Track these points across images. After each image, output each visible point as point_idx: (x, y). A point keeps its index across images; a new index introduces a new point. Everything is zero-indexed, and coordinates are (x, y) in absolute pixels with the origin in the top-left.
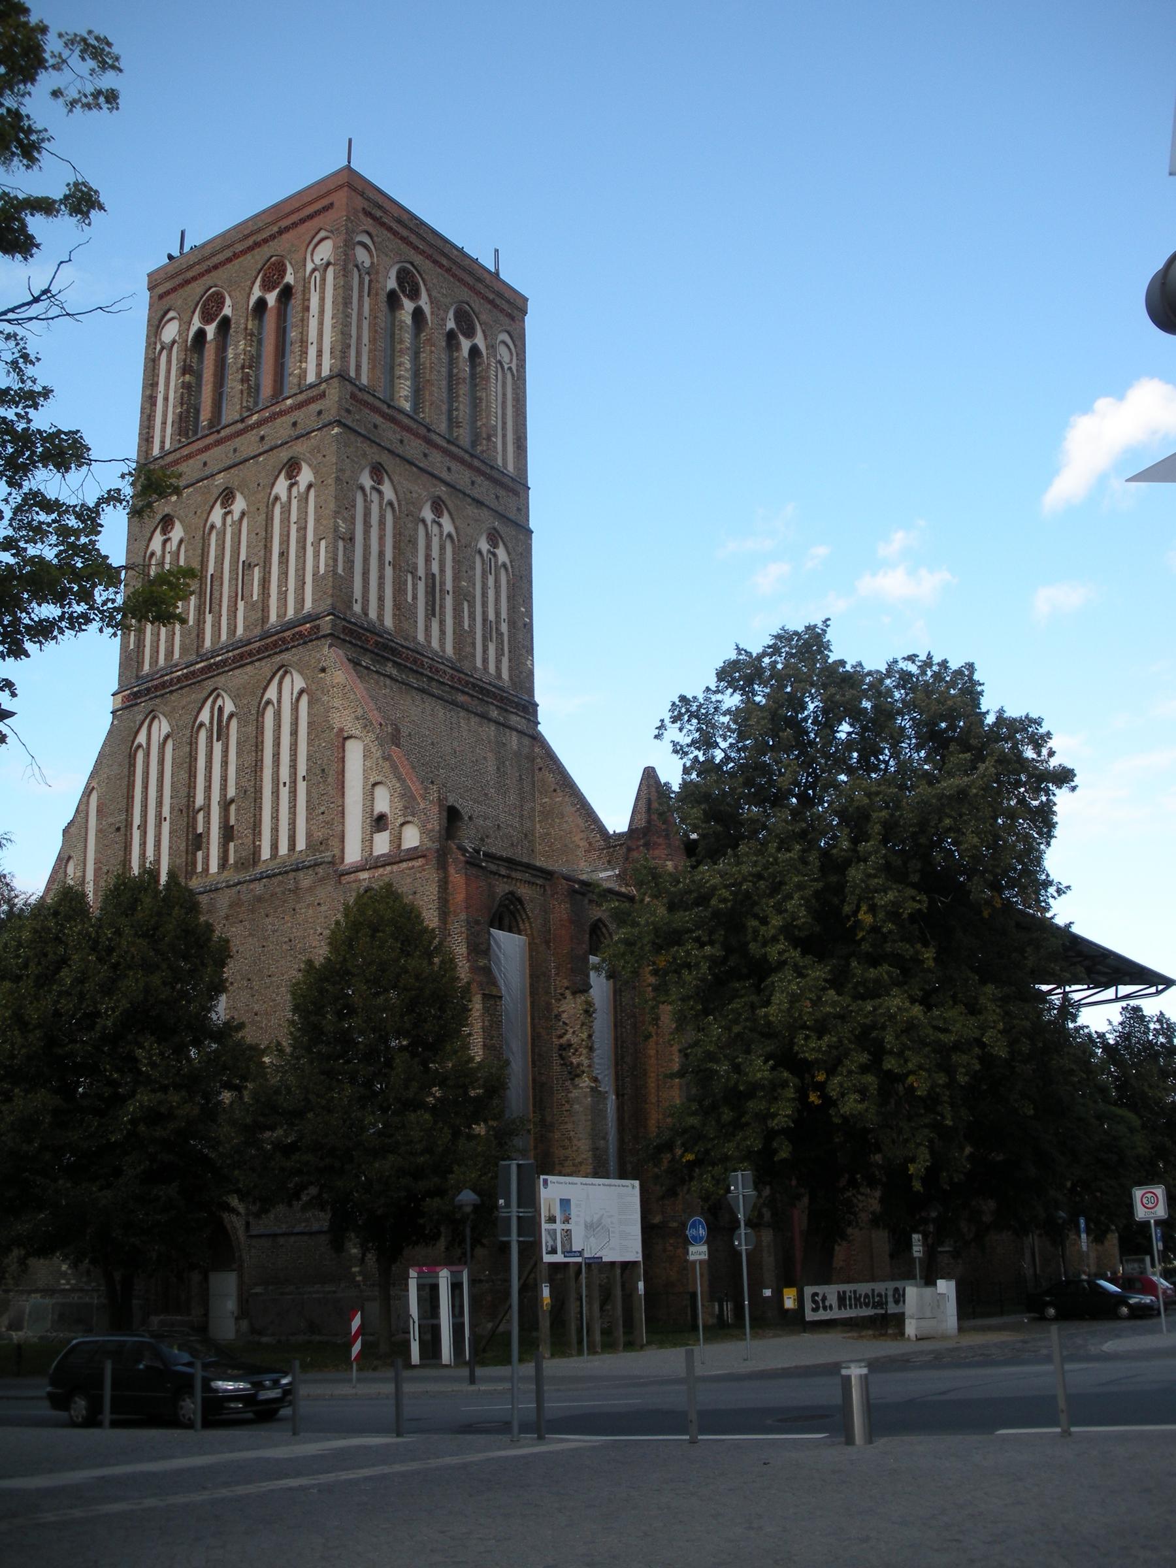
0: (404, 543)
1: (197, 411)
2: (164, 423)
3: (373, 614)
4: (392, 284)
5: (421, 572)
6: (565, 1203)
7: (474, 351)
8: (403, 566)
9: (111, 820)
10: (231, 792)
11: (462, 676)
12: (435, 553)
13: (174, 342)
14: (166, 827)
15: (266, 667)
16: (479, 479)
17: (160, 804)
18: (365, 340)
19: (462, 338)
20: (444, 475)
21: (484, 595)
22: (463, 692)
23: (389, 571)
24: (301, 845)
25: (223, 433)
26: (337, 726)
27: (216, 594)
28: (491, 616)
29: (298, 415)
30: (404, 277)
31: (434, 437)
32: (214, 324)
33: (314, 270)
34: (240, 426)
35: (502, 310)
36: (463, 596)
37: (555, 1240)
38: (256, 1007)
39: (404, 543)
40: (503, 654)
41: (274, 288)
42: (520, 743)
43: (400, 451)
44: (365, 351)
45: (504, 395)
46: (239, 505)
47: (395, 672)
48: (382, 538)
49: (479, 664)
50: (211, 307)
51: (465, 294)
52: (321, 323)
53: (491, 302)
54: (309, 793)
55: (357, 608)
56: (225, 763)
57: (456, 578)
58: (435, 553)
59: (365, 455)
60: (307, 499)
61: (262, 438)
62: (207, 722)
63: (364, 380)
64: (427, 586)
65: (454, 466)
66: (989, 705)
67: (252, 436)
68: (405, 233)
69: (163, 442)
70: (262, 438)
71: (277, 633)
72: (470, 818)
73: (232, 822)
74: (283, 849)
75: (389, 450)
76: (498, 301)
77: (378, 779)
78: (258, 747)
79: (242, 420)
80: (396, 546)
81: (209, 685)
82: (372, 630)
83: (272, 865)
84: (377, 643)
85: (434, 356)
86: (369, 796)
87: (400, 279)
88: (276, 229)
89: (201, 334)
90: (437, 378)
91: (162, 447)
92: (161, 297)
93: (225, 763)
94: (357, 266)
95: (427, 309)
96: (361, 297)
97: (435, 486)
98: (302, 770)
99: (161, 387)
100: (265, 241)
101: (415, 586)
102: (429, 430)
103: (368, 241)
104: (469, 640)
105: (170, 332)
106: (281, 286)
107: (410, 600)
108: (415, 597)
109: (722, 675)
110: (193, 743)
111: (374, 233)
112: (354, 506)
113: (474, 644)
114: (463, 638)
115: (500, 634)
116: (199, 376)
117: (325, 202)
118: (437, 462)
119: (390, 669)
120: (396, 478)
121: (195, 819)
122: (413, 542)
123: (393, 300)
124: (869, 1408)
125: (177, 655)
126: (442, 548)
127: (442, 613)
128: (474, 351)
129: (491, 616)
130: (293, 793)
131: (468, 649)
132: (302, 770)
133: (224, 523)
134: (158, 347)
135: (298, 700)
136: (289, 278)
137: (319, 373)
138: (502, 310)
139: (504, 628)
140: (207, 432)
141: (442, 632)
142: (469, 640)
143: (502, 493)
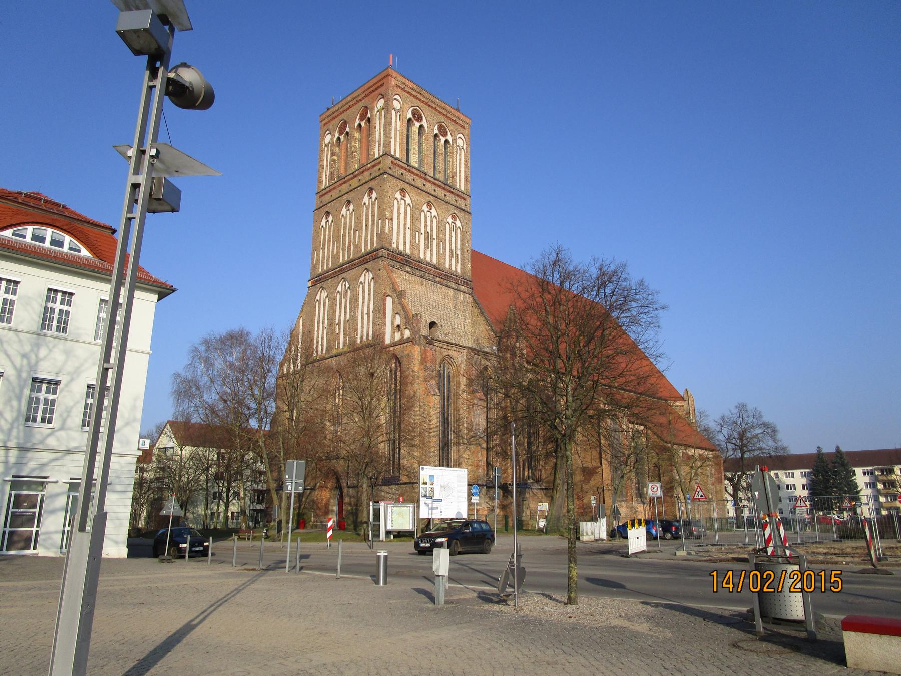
0: (415, 220)
5: (423, 231)
7: (447, 142)
8: (415, 229)
10: (348, 318)
16: (448, 194)
18: (398, 139)
20: (433, 193)
23: (408, 231)
28: (453, 248)
29: (372, 170)
35: (459, 125)
36: (440, 240)
39: (415, 220)
51: (442, 119)
55: (395, 246)
57: (438, 233)
63: (398, 156)
74: (365, 339)
78: (357, 300)
80: (412, 222)
82: (400, 254)
85: (428, 145)
86: (393, 318)
96: (396, 121)
101: (419, 237)
108: (419, 241)
110: (335, 299)
117: (381, 83)
119: (408, 269)
122: (419, 220)
126: (432, 222)
127: (432, 248)
128: (447, 142)
129: (453, 248)
130: (369, 317)
131: (442, 261)
132: (372, 310)
136: (369, 115)
138: (459, 125)
139: (459, 252)
141: (432, 255)
143: (458, 199)
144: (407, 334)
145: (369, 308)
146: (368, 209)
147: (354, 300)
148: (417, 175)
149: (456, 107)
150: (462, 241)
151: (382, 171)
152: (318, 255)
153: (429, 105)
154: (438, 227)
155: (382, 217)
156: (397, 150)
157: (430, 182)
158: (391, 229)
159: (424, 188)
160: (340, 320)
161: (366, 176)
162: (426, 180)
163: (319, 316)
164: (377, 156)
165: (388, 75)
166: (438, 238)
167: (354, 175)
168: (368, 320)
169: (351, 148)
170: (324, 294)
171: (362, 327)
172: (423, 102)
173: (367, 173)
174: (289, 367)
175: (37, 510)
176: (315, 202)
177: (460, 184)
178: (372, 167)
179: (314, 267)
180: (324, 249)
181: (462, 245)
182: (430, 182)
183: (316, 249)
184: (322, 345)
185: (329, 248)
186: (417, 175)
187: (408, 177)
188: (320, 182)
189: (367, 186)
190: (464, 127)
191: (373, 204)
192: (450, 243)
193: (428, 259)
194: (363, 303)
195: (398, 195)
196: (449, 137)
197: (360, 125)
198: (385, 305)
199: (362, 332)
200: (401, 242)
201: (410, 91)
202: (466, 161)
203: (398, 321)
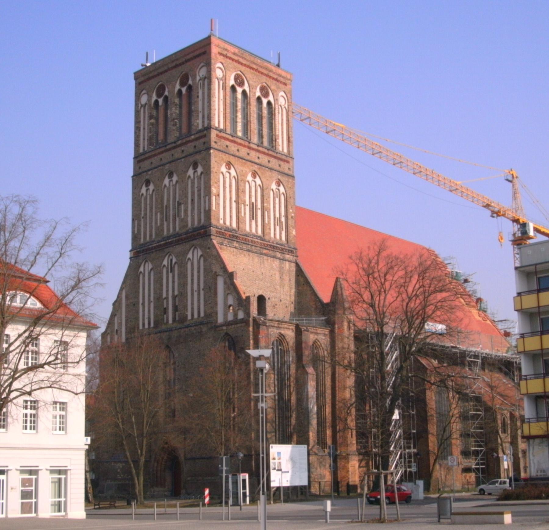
1: (157, 134)
2: (144, 139)
4: (232, 82)
5: (247, 202)
6: (279, 453)
7: (269, 103)
9: (131, 301)
10: (176, 293)
11: (265, 242)
13: (146, 104)
14: (152, 305)
15: (187, 246)
16: (272, 159)
17: (149, 296)
20: (257, 161)
21: (274, 207)
22: (265, 249)
24: (202, 315)
25: (168, 147)
26: (214, 271)
27: (168, 214)
29: (196, 143)
30: (237, 78)
33: (200, 80)
34: (174, 145)
35: (281, 82)
37: (275, 465)
38: (187, 375)
40: (283, 230)
42: (290, 266)
45: (282, 120)
46: (175, 178)
47: (237, 245)
50: (160, 92)
51: (264, 79)
52: (203, 104)
53: (276, 80)
54: (205, 295)
55: (221, 222)
56: (173, 282)
57: (263, 202)
59: (223, 159)
60: (201, 178)
61: (183, 151)
62: (166, 265)
63: (222, 127)
64: (250, 208)
65: (261, 156)
66: (449, 269)
67: (179, 150)
69: (144, 147)
70: (183, 151)
71: (191, 232)
72: (269, 299)
73: (177, 304)
74: (196, 316)
75: (233, 155)
76: (279, 78)
77: (229, 292)
78: (185, 276)
79: (175, 142)
81: (167, 250)
82: (227, 229)
83: (192, 322)
84: (230, 235)
87: (236, 79)
88: (184, 60)
89: (157, 102)
91: (144, 149)
93: (173, 282)
97: (252, 166)
98: (202, 286)
99: (142, 123)
101: (245, 209)
103: (221, 66)
104: (268, 227)
105: (144, 99)
106: (187, 85)
108: (245, 214)
110: (161, 273)
111: (224, 62)
112: (219, 182)
113: (270, 229)
115: (281, 222)
116: (157, 119)
119: (235, 244)
120: (236, 166)
121: (163, 302)
122: (244, 191)
124: (330, 516)
125: (154, 237)
128: (269, 103)
132: (202, 286)
133: (170, 185)
134: (140, 105)
135: (200, 259)
136: (190, 82)
137: (203, 126)
138: (281, 82)
139: (283, 219)
140: (161, 145)
141: (257, 225)
142: (268, 227)
143: (281, 163)
146: (193, 182)
147: (183, 275)
149: (276, 63)
153: (251, 68)
158: (218, 204)
159: (248, 158)
160: (167, 294)
161: (189, 148)
162: (250, 148)
163: (144, 289)
164: (200, 127)
166: (263, 207)
170: (149, 266)
171: (192, 304)
172: (245, 65)
174: (112, 339)
175: (33, 488)
178: (197, 139)
180: (145, 217)
184: (149, 319)
185: (151, 218)
187: (233, 148)
189: (192, 159)
191: (200, 178)
193: (252, 184)
194: (192, 280)
195: (224, 169)
196: (271, 98)
197: (180, 91)
198: (216, 284)
199: (192, 309)
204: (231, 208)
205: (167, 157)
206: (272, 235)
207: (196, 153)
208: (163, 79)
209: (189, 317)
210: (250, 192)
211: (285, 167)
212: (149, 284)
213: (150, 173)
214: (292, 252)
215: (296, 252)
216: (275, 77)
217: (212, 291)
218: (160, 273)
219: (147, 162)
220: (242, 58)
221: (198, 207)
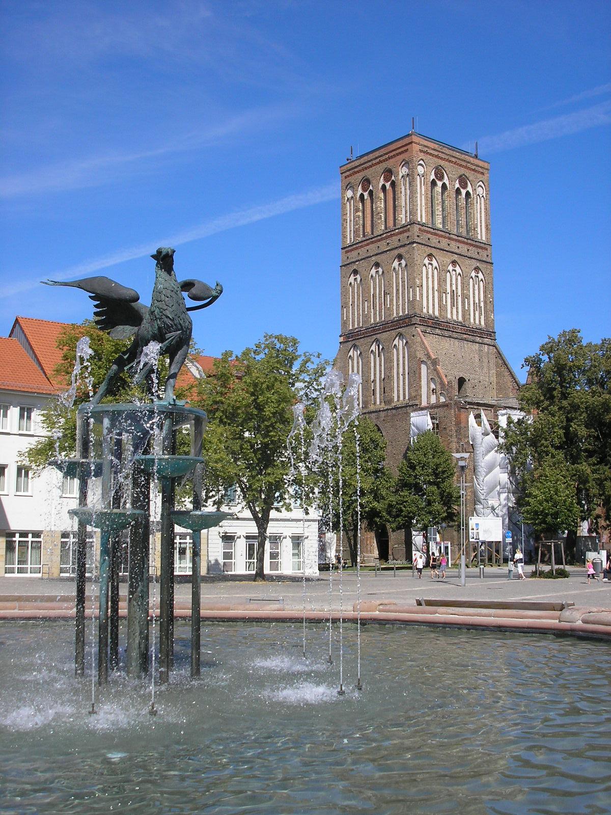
0: (442, 281)
3: (431, 312)
5: (449, 290)
6: (477, 525)
7: (468, 194)
8: (442, 291)
12: (454, 282)
18: (423, 204)
19: (462, 190)
21: (474, 294)
22: (465, 334)
23: (436, 293)
28: (477, 301)
31: (452, 236)
32: (367, 192)
36: (465, 297)
39: (442, 281)
41: (389, 181)
43: (438, 246)
44: (424, 208)
48: (433, 282)
49: (472, 320)
50: (366, 182)
51: (462, 171)
53: (474, 170)
55: (425, 311)
57: (463, 289)
58: (454, 282)
63: (424, 221)
65: (460, 245)
68: (436, 153)
74: (401, 398)
78: (392, 361)
80: (439, 284)
82: (431, 318)
85: (450, 202)
90: (452, 210)
92: (346, 177)
94: (418, 175)
95: (447, 183)
96: (421, 187)
97: (453, 256)
100: (384, 161)
101: (446, 297)
102: (450, 234)
107: (444, 303)
108: (446, 302)
109: (542, 348)
113: (470, 314)
114: (465, 313)
115: (480, 307)
117: (405, 148)
118: (454, 246)
122: (445, 281)
123: (434, 183)
126: (457, 279)
127: (457, 305)
128: (468, 194)
129: (477, 301)
131: (468, 317)
139: (482, 304)
141: (457, 312)
143: (480, 250)
144: (442, 399)
145: (404, 369)
147: (389, 361)
148: (442, 236)
150: (485, 292)
151: (410, 240)
152: (348, 312)
153: (450, 161)
154: (462, 283)
155: (412, 286)
156: (422, 216)
157: (453, 240)
158: (421, 295)
161: (394, 241)
165: (411, 143)
166: (463, 294)
167: (380, 238)
168: (404, 381)
169: (376, 208)
173: (395, 238)
176: (338, 258)
177: (481, 235)
178: (401, 233)
179: (345, 324)
181: (485, 296)
182: (453, 240)
183: (344, 306)
186: (442, 236)
187: (434, 240)
188: (345, 237)
189: (396, 252)
190: (483, 174)
192: (474, 297)
193: (455, 317)
196: (469, 188)
200: (429, 306)
201: (432, 152)
202: (486, 209)
203: (433, 386)
204: (433, 297)
205: (373, 249)
206: (472, 320)
207: (401, 246)
208: (368, 173)
209: (396, 399)
210: (451, 281)
211: (483, 255)
212: (375, 366)
213: (357, 263)
214: (490, 335)
215: (495, 335)
216: (474, 167)
217: (417, 375)
218: (368, 357)
219: (355, 253)
220: (442, 152)
221: (399, 294)
